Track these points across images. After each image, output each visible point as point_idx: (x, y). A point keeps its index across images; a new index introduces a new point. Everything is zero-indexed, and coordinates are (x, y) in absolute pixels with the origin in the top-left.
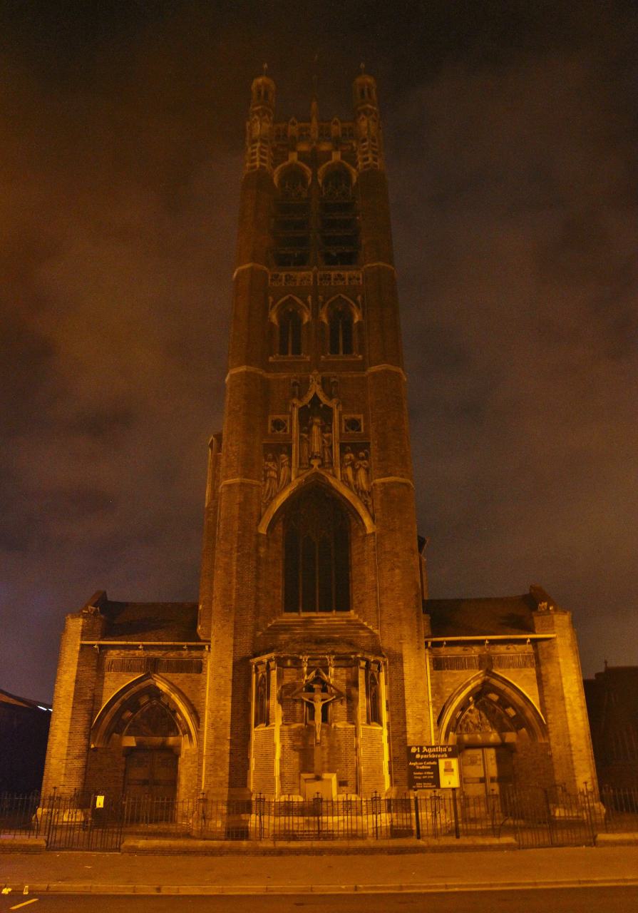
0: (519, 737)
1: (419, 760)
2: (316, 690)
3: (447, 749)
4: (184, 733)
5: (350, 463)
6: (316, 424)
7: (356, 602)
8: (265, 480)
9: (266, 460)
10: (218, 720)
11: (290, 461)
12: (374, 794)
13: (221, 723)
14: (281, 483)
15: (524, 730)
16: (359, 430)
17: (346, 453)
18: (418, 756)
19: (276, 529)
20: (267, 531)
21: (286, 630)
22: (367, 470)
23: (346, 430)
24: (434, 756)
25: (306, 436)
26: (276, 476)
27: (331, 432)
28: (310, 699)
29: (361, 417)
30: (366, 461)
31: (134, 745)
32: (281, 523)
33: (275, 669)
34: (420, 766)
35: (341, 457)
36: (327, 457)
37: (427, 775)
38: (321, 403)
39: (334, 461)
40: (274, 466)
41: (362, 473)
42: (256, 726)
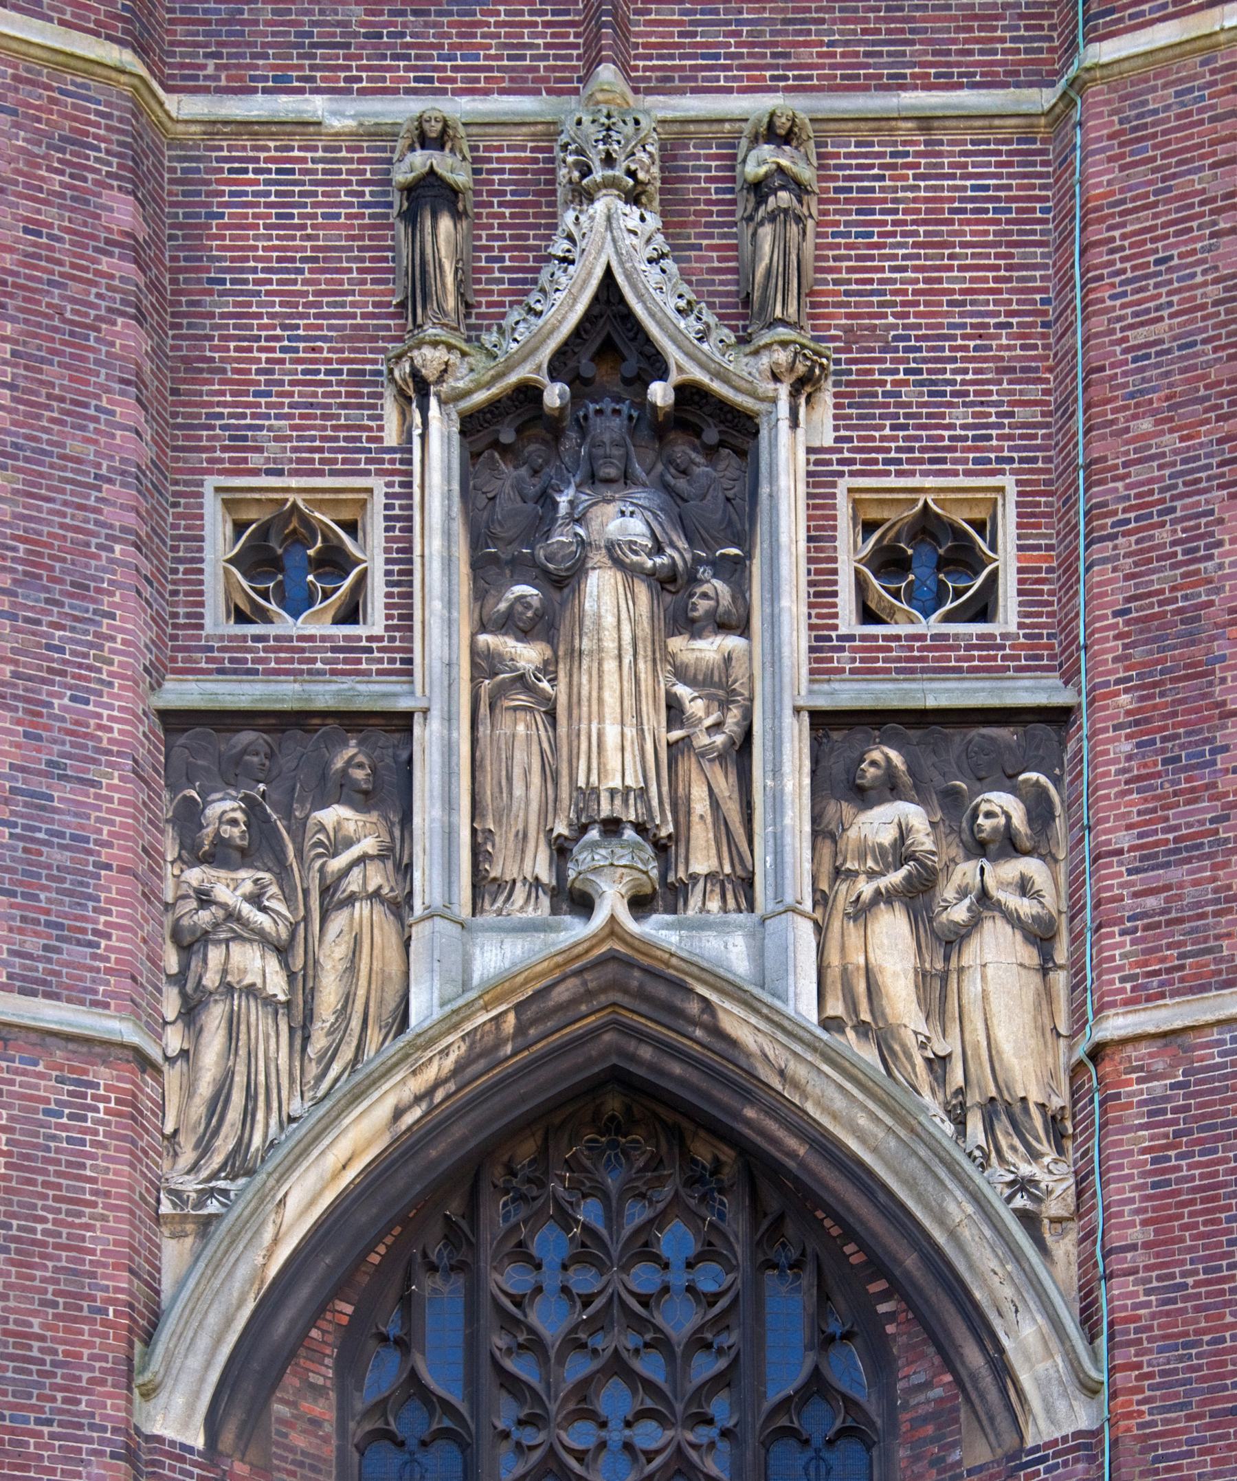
5: (896, 877)
6: (616, 556)
8: (191, 1012)
9: (194, 855)
14: (319, 1042)
16: (982, 609)
17: (863, 797)
19: (278, 1408)
23: (868, 615)
25: (528, 655)
26: (277, 985)
30: (1031, 867)
32: (323, 1374)
36: (702, 835)
38: (657, 366)
39: (762, 862)
40: (255, 899)
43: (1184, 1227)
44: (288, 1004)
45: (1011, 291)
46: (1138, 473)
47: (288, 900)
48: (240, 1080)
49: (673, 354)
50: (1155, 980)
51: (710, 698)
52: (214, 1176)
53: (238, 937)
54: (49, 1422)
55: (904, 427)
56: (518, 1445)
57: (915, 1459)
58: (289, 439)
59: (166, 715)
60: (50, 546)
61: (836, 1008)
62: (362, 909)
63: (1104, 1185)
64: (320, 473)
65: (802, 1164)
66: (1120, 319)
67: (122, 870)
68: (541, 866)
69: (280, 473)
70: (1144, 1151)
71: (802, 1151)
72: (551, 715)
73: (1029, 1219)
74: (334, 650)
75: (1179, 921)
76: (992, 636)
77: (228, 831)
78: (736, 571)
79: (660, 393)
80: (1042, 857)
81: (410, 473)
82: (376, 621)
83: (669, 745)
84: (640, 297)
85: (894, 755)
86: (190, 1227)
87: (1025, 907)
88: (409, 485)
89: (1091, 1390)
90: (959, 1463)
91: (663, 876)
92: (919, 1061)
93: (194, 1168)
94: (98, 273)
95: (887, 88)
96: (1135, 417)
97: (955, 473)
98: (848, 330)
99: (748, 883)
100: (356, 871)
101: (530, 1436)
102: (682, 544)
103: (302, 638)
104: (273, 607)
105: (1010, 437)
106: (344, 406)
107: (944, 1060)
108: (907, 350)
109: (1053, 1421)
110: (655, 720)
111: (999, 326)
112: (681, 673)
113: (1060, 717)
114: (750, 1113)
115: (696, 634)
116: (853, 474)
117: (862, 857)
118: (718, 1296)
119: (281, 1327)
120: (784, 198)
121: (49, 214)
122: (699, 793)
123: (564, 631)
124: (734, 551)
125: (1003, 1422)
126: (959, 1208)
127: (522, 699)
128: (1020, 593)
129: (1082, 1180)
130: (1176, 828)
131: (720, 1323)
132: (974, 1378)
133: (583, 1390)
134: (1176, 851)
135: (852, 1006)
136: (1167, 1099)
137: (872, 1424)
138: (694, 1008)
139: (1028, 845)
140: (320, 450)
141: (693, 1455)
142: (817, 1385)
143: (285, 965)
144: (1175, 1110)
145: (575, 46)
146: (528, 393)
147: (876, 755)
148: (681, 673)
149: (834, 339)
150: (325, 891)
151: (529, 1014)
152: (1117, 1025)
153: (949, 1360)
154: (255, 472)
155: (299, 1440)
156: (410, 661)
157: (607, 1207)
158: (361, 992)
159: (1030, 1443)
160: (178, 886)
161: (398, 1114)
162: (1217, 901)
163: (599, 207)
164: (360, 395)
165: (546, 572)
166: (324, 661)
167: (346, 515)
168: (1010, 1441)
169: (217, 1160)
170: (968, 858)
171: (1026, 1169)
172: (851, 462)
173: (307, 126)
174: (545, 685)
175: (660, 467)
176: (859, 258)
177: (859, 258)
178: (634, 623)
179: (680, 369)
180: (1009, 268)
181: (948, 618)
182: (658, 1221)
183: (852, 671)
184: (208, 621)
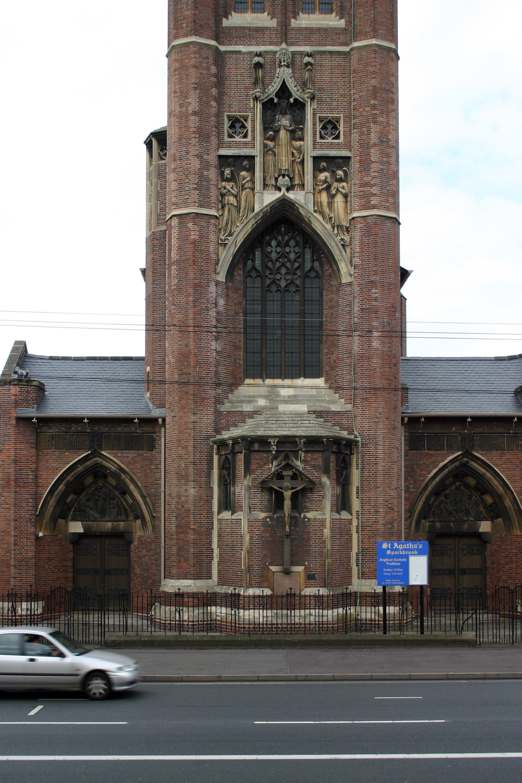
0: (494, 527)
1: (390, 557)
2: (285, 477)
3: (418, 546)
4: (137, 517)
5: (325, 186)
7: (326, 368)
8: (223, 207)
9: (223, 180)
10: (180, 506)
11: (253, 181)
12: (289, 590)
13: (183, 510)
15: (500, 520)
18: (389, 552)
19: (235, 273)
20: (226, 278)
21: (249, 402)
22: (346, 196)
24: (404, 553)
25: (271, 144)
26: (235, 204)
27: (302, 139)
28: (279, 488)
29: (341, 140)
30: (344, 184)
31: (82, 531)
33: (241, 452)
34: (390, 562)
35: (315, 177)
36: (297, 177)
37: (397, 572)
38: (291, 95)
40: (232, 188)
41: (339, 199)
42: (219, 513)
43: (365, 250)
44: (237, 206)
45: (342, 82)
46: (360, 118)
47: (237, 188)
48: (230, 220)
49: (293, 94)
50: (362, 207)
51: (298, 152)
52: (226, 236)
53: (230, 195)
54: (205, 280)
55: (327, 105)
56: (269, 278)
57: (326, 282)
58: (237, 106)
59: (220, 157)
60: (203, 129)
61: (316, 209)
62: (248, 190)
63: (354, 241)
64: (241, 112)
65: (311, 233)
66: (358, 91)
67: (214, 185)
68: (273, 182)
69: (236, 112)
70: (360, 236)
71: (311, 232)
72: (275, 155)
73: (343, 246)
74: (244, 143)
75: (365, 197)
76: (339, 143)
77: (228, 176)
78: (302, 130)
79: (292, 100)
80: (346, 182)
81: (255, 112)
82: (249, 139)
83: (292, 161)
84: (289, 84)
85: (325, 164)
86: (223, 245)
87: (344, 191)
88: (255, 114)
89: (351, 275)
90: (332, 284)
91: (291, 184)
92: (328, 218)
93: (224, 235)
94: (210, 81)
95: (324, 46)
96: (360, 108)
97: (334, 114)
98: (319, 88)
99: (303, 185)
100: (247, 183)
101: (271, 277)
102: (294, 125)
103: (239, 141)
104: (234, 135)
105: (342, 108)
106: (245, 100)
107: (332, 217)
108: (327, 92)
109: (346, 280)
110: (290, 156)
111: (341, 88)
112: (294, 148)
113: (349, 158)
114: (303, 225)
115: (296, 141)
116: (319, 113)
117: (320, 182)
118: (298, 253)
119: (236, 261)
120: (309, 67)
121: (204, 71)
122: (296, 169)
123: (277, 140)
124: (302, 126)
125: (339, 278)
126: (333, 244)
127: (271, 153)
128: (343, 135)
129: (351, 239)
130: (365, 181)
131: (298, 257)
132: (335, 270)
133: (279, 269)
134: (365, 185)
135: (318, 208)
136: (363, 228)
137: (320, 275)
138: (296, 208)
139: (344, 180)
140: (241, 108)
141: (294, 280)
142: (312, 268)
143: (236, 199)
144: (364, 230)
145: (279, 37)
146: (272, 99)
147: (322, 164)
148: (294, 148)
149: (317, 89)
150: (242, 186)
151: (272, 208)
152: (355, 214)
153: (331, 267)
154: (232, 112)
155: (238, 278)
156: (254, 146)
157: (291, 263)
158: (248, 205)
159: (343, 282)
160: (221, 185)
161: (253, 225)
162: (370, 194)
163: (282, 68)
164: (247, 98)
165: (274, 130)
166: (242, 146)
167: (245, 119)
168: (340, 281)
169: (227, 234)
170: (335, 182)
171: (343, 237)
172: (319, 111)
173: (239, 52)
174: (274, 150)
175: (291, 111)
176: (321, 75)
177: (321, 75)
178: (287, 140)
179: (294, 96)
180: (342, 78)
181: (333, 139)
182: (289, 240)
183: (319, 148)
184: (225, 138)
